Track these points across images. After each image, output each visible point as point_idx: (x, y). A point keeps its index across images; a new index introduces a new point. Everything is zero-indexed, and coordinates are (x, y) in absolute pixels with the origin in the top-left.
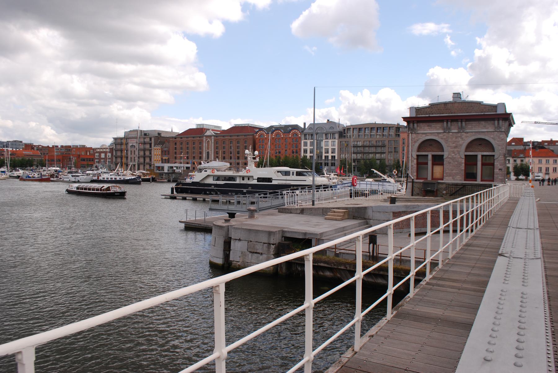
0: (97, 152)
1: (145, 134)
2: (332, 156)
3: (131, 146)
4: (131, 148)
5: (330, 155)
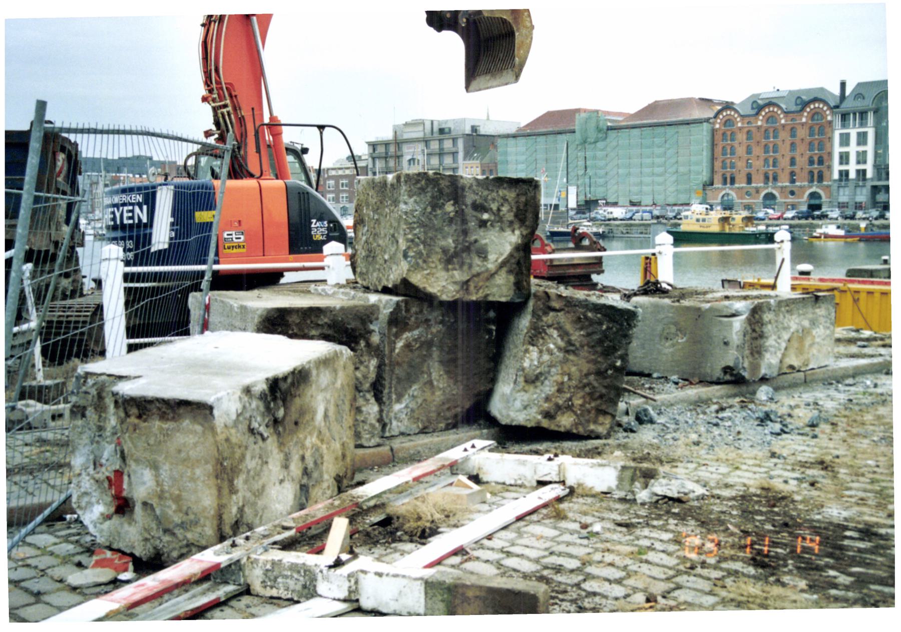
0: (330, 178)
1: (442, 131)
2: (858, 171)
3: (410, 161)
4: (410, 164)
5: (852, 168)
